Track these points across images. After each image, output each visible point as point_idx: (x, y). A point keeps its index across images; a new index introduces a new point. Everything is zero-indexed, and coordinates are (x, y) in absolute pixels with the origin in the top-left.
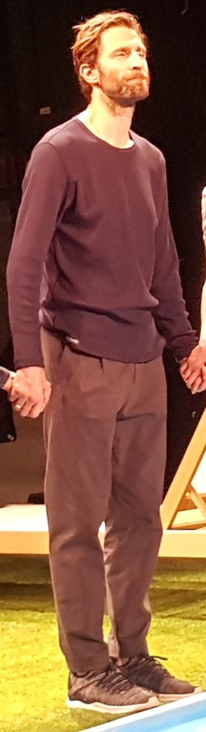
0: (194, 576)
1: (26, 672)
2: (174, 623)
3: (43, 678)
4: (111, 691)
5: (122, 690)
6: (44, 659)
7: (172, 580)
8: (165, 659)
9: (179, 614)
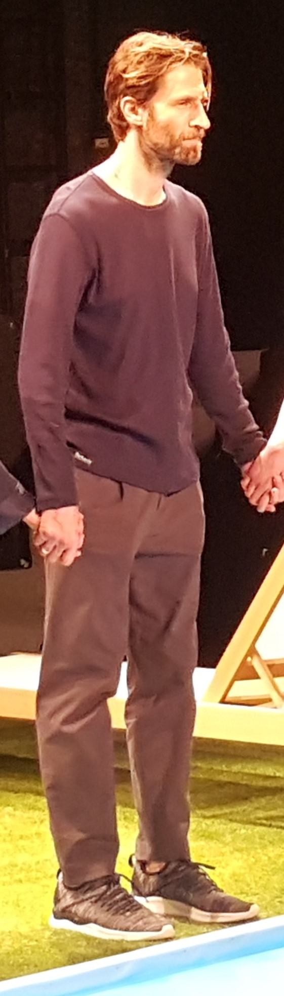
0: (250, 766)
1: (22, 876)
2: (217, 826)
3: (43, 886)
4: (112, 911)
5: (128, 910)
6: (46, 860)
7: (219, 768)
8: (213, 868)
9: (226, 814)
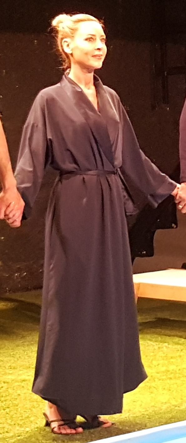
1: (172, 376)
